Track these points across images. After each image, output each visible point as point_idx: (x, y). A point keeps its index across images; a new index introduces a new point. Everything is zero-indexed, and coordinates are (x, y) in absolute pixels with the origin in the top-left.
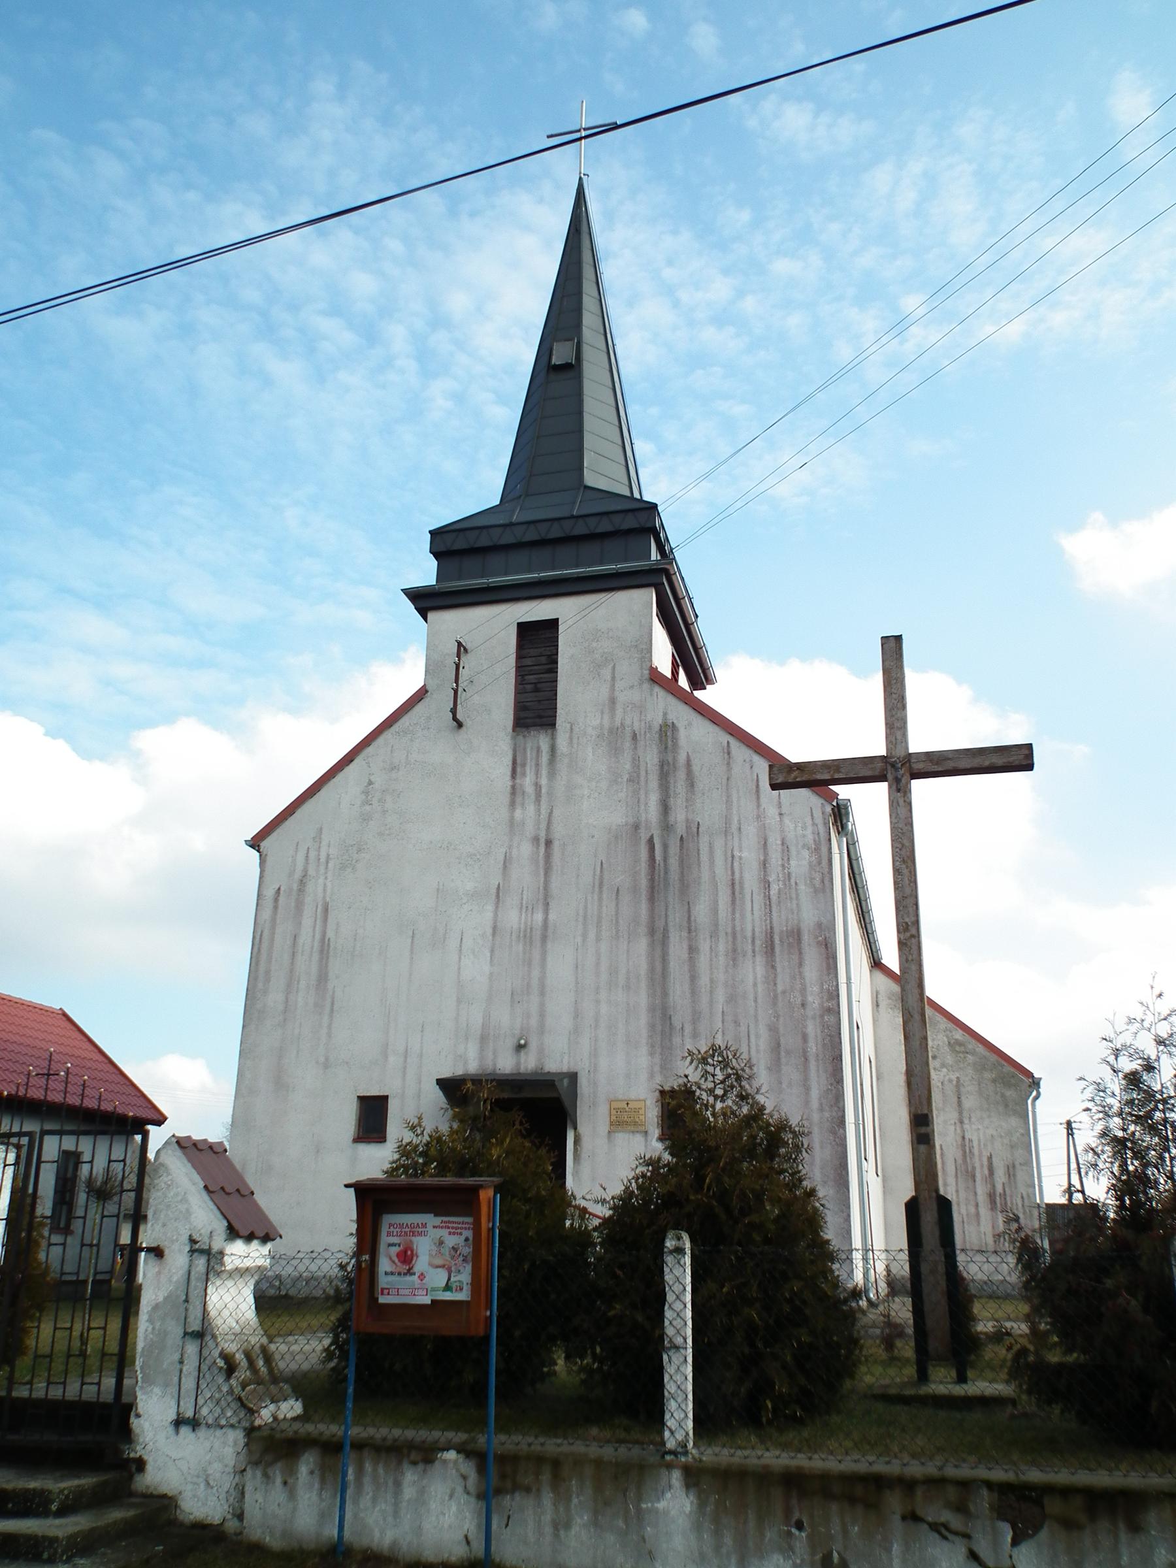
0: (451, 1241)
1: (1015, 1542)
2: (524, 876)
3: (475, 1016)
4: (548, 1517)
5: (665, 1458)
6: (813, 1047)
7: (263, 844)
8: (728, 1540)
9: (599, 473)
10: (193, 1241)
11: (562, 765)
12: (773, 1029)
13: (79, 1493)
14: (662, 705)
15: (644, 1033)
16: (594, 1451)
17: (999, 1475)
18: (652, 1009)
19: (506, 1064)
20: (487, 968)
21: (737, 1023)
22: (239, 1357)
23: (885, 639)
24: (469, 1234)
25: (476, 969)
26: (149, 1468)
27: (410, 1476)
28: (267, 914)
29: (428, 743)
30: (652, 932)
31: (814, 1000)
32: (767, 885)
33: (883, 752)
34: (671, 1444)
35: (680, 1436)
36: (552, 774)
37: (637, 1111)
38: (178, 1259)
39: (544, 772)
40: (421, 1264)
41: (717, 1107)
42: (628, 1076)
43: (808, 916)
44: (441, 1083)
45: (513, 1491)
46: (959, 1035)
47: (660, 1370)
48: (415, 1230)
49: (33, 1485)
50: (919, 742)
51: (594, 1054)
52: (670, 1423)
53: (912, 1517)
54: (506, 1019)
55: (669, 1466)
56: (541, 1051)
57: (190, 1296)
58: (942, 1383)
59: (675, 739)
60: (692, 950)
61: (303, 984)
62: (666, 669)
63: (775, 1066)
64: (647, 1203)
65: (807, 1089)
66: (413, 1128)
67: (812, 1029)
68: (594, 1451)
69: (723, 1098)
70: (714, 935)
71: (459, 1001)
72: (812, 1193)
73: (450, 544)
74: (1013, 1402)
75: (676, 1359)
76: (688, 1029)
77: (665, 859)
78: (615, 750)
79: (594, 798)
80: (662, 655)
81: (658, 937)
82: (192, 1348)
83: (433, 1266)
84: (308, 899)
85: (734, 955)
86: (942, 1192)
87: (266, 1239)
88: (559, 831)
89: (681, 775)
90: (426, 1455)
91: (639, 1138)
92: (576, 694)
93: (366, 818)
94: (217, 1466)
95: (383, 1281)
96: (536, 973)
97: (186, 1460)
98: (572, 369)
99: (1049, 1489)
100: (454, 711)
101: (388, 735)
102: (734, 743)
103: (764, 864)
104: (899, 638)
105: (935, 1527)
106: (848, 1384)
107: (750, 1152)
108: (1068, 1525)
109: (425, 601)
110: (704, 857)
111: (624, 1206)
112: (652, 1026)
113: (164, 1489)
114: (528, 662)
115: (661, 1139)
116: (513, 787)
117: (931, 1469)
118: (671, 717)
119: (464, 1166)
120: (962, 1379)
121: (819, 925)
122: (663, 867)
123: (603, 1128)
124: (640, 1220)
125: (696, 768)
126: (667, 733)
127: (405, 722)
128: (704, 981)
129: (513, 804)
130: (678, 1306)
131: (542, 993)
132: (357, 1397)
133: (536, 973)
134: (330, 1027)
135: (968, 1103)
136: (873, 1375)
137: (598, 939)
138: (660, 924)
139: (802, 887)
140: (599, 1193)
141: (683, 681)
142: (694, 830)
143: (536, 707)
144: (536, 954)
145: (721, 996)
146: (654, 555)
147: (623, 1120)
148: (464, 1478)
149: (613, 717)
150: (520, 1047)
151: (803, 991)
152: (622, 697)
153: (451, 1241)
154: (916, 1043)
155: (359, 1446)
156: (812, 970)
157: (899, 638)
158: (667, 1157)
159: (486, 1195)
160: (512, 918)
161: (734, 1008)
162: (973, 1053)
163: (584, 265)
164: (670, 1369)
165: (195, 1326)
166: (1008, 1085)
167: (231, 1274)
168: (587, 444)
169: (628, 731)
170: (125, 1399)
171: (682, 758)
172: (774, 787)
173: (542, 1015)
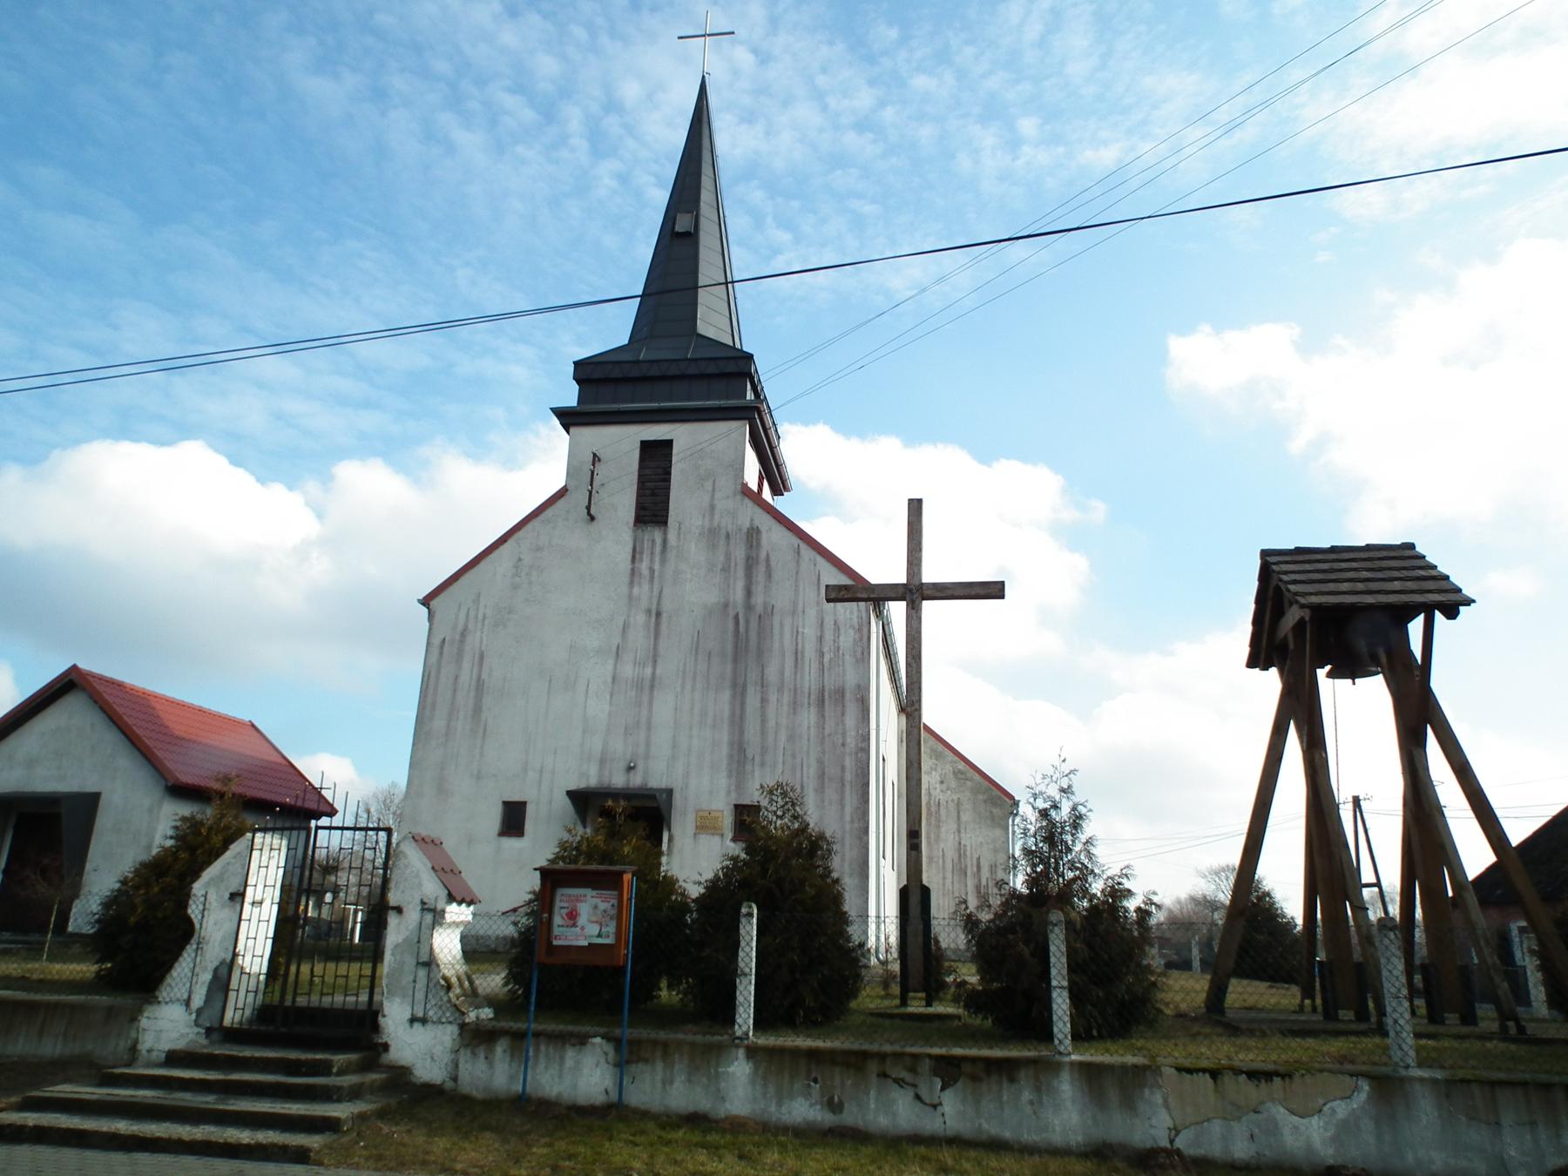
0: (603, 906)
1: (942, 1089)
2: (639, 639)
3: (596, 744)
4: (659, 1078)
5: (737, 1042)
6: (848, 776)
7: (433, 603)
8: (771, 1089)
9: (710, 324)
10: (423, 903)
11: (671, 555)
12: (820, 762)
13: (349, 1063)
14: (749, 514)
15: (725, 762)
16: (690, 1038)
17: (936, 1051)
18: (731, 744)
19: (618, 780)
20: (607, 708)
21: (794, 756)
22: (454, 980)
23: (911, 501)
24: (615, 902)
25: (599, 708)
26: (392, 1049)
27: (570, 1053)
28: (434, 659)
29: (566, 531)
30: (734, 685)
31: (851, 741)
32: (822, 655)
33: (904, 580)
34: (739, 1033)
35: (744, 1028)
36: (663, 561)
37: (716, 818)
38: (413, 915)
39: (657, 559)
40: (582, 920)
41: (777, 823)
42: (711, 793)
43: (851, 679)
44: (570, 793)
45: (637, 1062)
46: (961, 766)
47: (734, 987)
48: (578, 899)
49: (319, 1056)
50: (929, 575)
51: (687, 775)
52: (739, 1020)
53: (883, 1075)
54: (619, 747)
55: (737, 1046)
56: (646, 772)
57: (421, 939)
58: (916, 1007)
59: (764, 633)
60: (764, 701)
61: (462, 714)
62: (753, 485)
63: (820, 789)
64: (729, 883)
65: (843, 807)
66: (569, 831)
67: (849, 763)
68: (690, 1038)
69: (781, 818)
70: (780, 690)
71: (584, 732)
72: (837, 881)
73: (589, 373)
74: (959, 1017)
75: (745, 981)
76: (757, 759)
77: (747, 631)
78: (713, 547)
79: (694, 582)
80: (752, 470)
81: (739, 691)
82: (422, 973)
83: (589, 921)
84: (468, 648)
85: (795, 706)
86: (925, 882)
87: (469, 904)
88: (667, 605)
89: (762, 568)
90: (581, 1041)
91: (717, 839)
92: (683, 499)
93: (515, 587)
94: (439, 1048)
95: (556, 931)
96: (644, 712)
97: (418, 1044)
98: (690, 238)
99: (964, 1059)
100: (588, 508)
101: (535, 523)
102: (803, 546)
103: (821, 639)
104: (920, 501)
105: (896, 1081)
106: (853, 1004)
107: (798, 853)
108: (975, 1078)
109: (568, 418)
110: (776, 631)
111: (713, 887)
112: (731, 757)
113: (402, 1063)
114: (648, 472)
115: (734, 840)
116: (633, 570)
117: (897, 1048)
118: (757, 523)
119: (606, 857)
120: (929, 1004)
121: (859, 686)
122: (743, 639)
123: (690, 830)
124: (723, 897)
125: (773, 563)
126: (753, 535)
127: (549, 512)
128: (771, 723)
129: (632, 583)
130: (747, 949)
131: (649, 728)
132: (538, 1005)
133: (644, 712)
134: (482, 747)
135: (965, 817)
136: (869, 999)
137: (693, 690)
138: (741, 681)
139: (847, 657)
140: (698, 878)
141: (767, 494)
142: (770, 611)
143: (652, 508)
144: (645, 699)
145: (783, 737)
146: (750, 396)
147: (706, 825)
148: (606, 1054)
149: (712, 520)
150: (630, 769)
151: (844, 734)
152: (720, 505)
153: (603, 906)
154: (914, 783)
155: (537, 1035)
156: (851, 720)
157: (920, 501)
158: (743, 856)
159: (627, 877)
160: (628, 671)
161: (788, 761)
162: (971, 780)
163: (703, 178)
164: (740, 988)
165: (424, 958)
166: (994, 804)
167: (450, 925)
168: (700, 300)
169: (723, 532)
170: (375, 1007)
171: (763, 555)
172: (828, 601)
173: (648, 744)
